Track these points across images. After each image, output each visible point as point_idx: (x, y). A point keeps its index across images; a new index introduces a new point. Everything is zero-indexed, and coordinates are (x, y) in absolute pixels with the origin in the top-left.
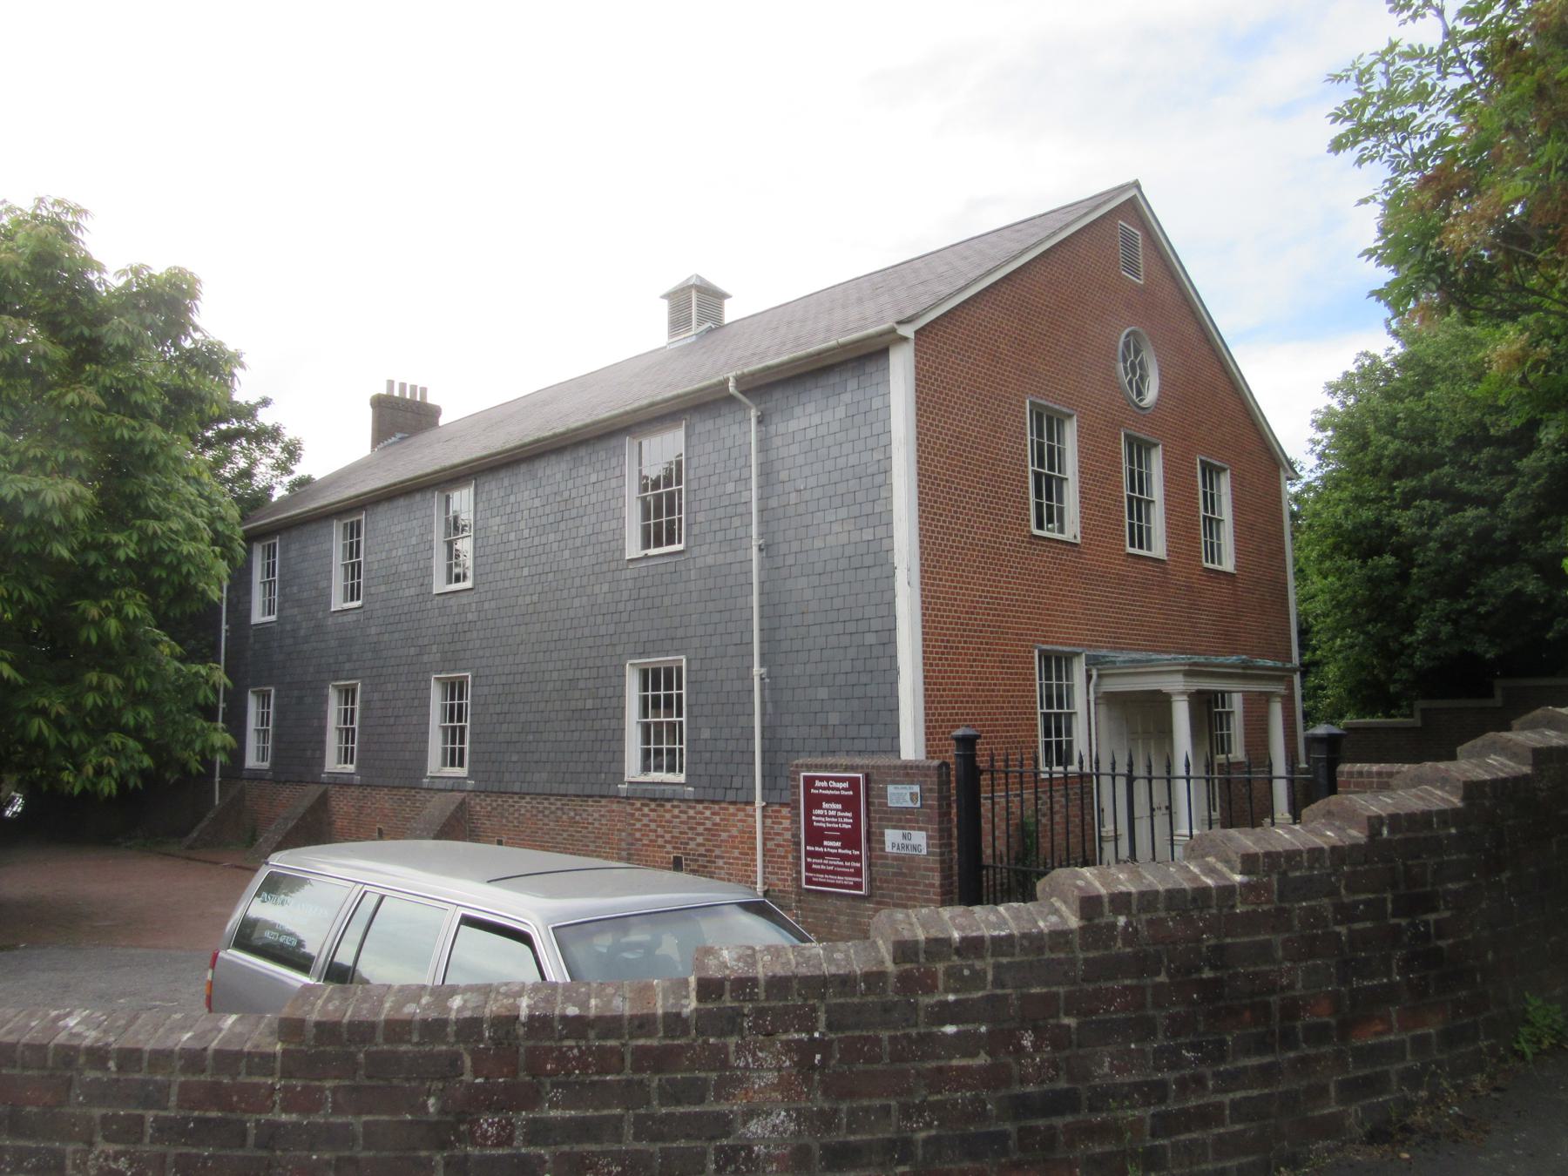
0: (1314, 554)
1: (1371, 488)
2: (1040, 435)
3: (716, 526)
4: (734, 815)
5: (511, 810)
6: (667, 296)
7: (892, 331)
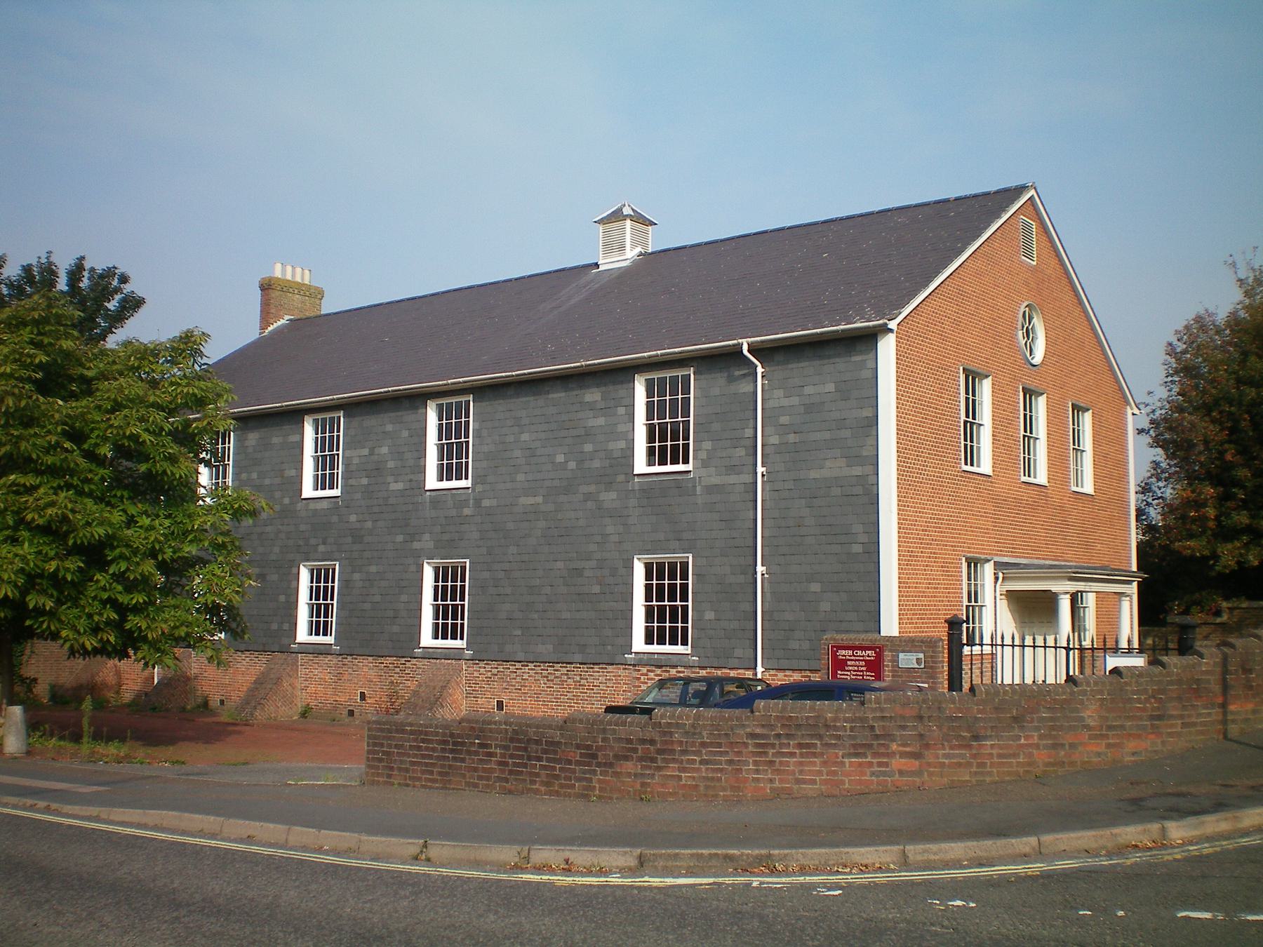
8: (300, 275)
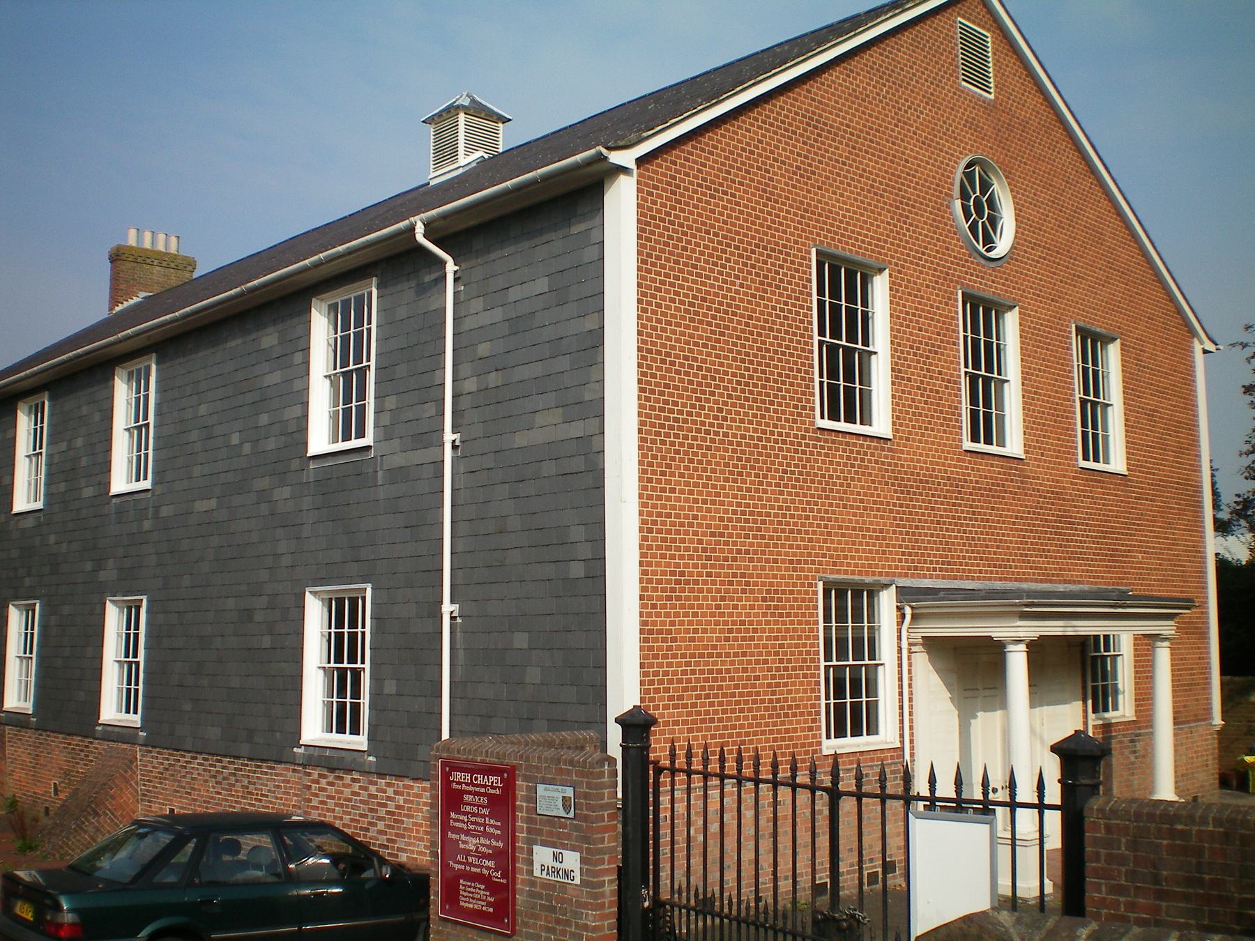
2: (975, 330)
8: (165, 243)
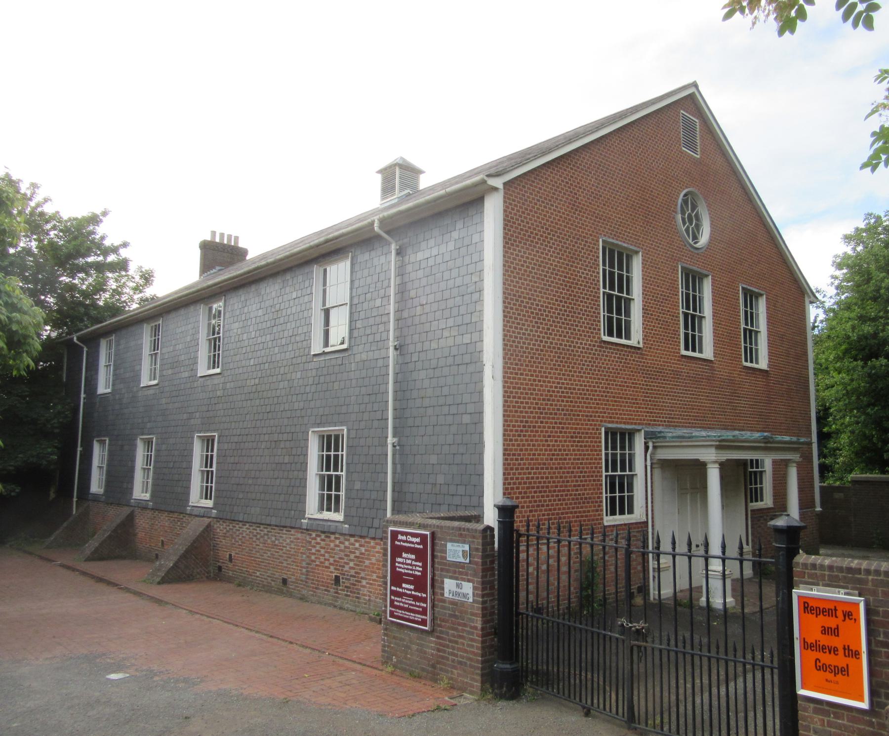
0: (832, 357)
1: (872, 310)
3: (368, 331)
4: (374, 548)
5: (238, 532)
6: (380, 172)
7: (484, 182)
